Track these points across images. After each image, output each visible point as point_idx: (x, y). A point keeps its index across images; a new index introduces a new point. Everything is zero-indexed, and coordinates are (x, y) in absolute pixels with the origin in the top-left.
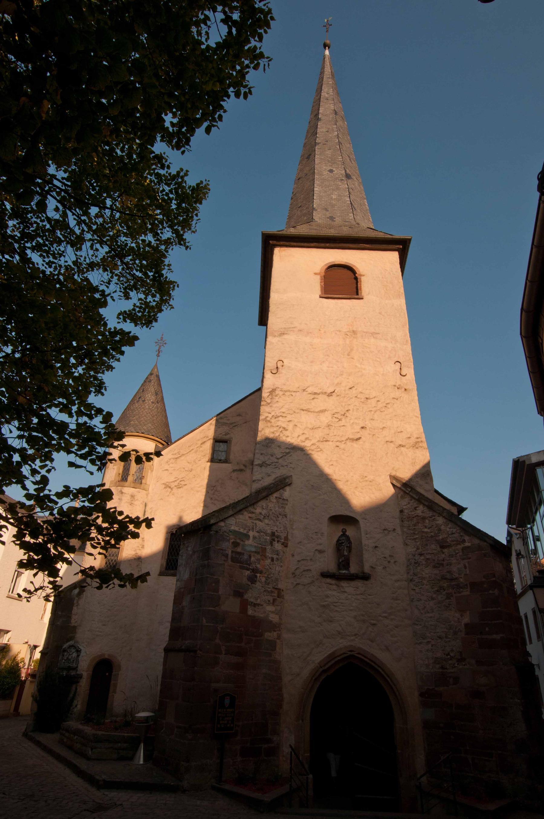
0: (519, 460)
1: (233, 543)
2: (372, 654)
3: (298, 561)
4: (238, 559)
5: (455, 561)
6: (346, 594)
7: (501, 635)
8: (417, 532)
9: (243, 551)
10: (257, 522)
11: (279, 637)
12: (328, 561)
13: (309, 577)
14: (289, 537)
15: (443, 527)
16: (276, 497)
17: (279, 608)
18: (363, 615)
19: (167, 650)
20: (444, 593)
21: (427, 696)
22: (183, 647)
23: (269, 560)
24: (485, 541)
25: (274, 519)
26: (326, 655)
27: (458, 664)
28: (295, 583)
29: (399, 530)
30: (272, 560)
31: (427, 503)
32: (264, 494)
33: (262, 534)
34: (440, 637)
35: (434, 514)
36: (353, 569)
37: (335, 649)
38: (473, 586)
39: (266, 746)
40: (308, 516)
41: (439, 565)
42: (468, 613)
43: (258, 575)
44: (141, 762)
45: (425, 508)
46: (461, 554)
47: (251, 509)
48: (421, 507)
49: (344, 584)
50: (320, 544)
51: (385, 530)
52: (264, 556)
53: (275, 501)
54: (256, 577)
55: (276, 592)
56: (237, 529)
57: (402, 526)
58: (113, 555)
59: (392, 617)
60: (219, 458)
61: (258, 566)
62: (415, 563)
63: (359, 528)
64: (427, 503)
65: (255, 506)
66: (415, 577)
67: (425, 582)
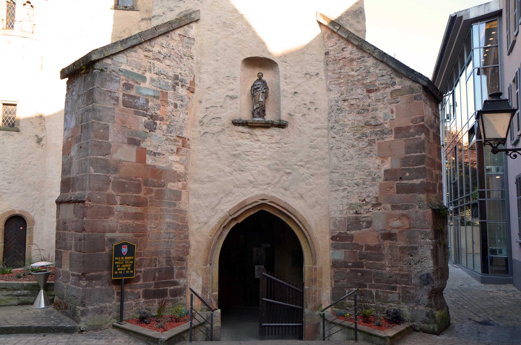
0: (456, 16)
1: (124, 85)
2: (285, 203)
3: (206, 108)
4: (130, 103)
5: (382, 106)
6: (259, 143)
7: (421, 180)
8: (342, 76)
9: (137, 95)
10: (156, 62)
11: (184, 187)
12: (243, 110)
13: (219, 125)
14: (196, 82)
15: (372, 70)
16: (180, 35)
17: (184, 158)
18: (277, 165)
19: (59, 202)
20: (366, 140)
21: (338, 240)
22: (72, 199)
23: (172, 107)
24: (418, 82)
25: (177, 60)
26: (236, 204)
27: (373, 209)
28: (203, 131)
29: (322, 75)
30: (176, 106)
31: (356, 43)
32: (163, 30)
33: (162, 76)
34: (357, 185)
35: (364, 54)
36: (269, 117)
37: (245, 198)
38: (399, 131)
39: (172, 288)
40: (219, 58)
41: (363, 111)
42: (389, 159)
43: (158, 122)
44: (43, 305)
45: (355, 48)
46: (389, 97)
47: (146, 46)
48: (350, 48)
49: (258, 132)
50: (232, 90)
51: (306, 74)
52: (166, 102)
53: (178, 38)
54: (156, 124)
55: (181, 141)
56: (129, 69)
57: (326, 70)
58: (10, 113)
59: (309, 166)
60: (125, 5)
61: (158, 112)
62: (337, 109)
63: (277, 73)
64: (356, 43)
65: (153, 43)
66: (337, 125)
67: (347, 129)
